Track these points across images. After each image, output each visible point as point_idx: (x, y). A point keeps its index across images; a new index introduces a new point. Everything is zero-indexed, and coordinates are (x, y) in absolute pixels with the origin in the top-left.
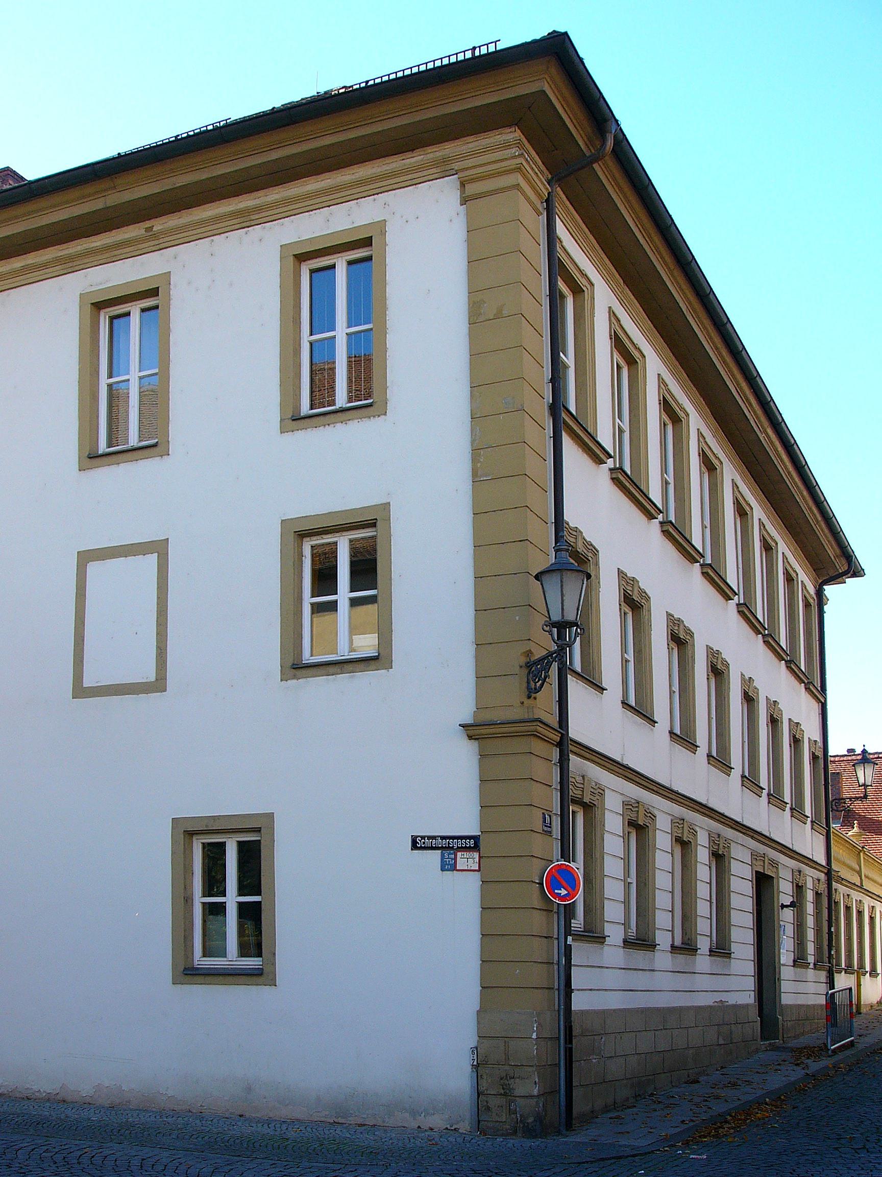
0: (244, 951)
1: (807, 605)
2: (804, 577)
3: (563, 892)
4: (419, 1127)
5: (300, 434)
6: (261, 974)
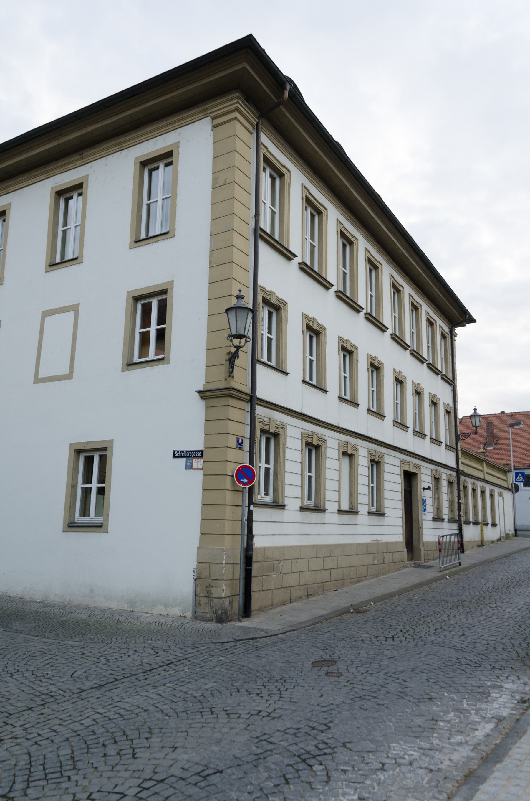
0: (96, 515)
1: (443, 336)
2: (440, 324)
3: (245, 481)
4: (168, 614)
5: (138, 249)
6: (101, 526)
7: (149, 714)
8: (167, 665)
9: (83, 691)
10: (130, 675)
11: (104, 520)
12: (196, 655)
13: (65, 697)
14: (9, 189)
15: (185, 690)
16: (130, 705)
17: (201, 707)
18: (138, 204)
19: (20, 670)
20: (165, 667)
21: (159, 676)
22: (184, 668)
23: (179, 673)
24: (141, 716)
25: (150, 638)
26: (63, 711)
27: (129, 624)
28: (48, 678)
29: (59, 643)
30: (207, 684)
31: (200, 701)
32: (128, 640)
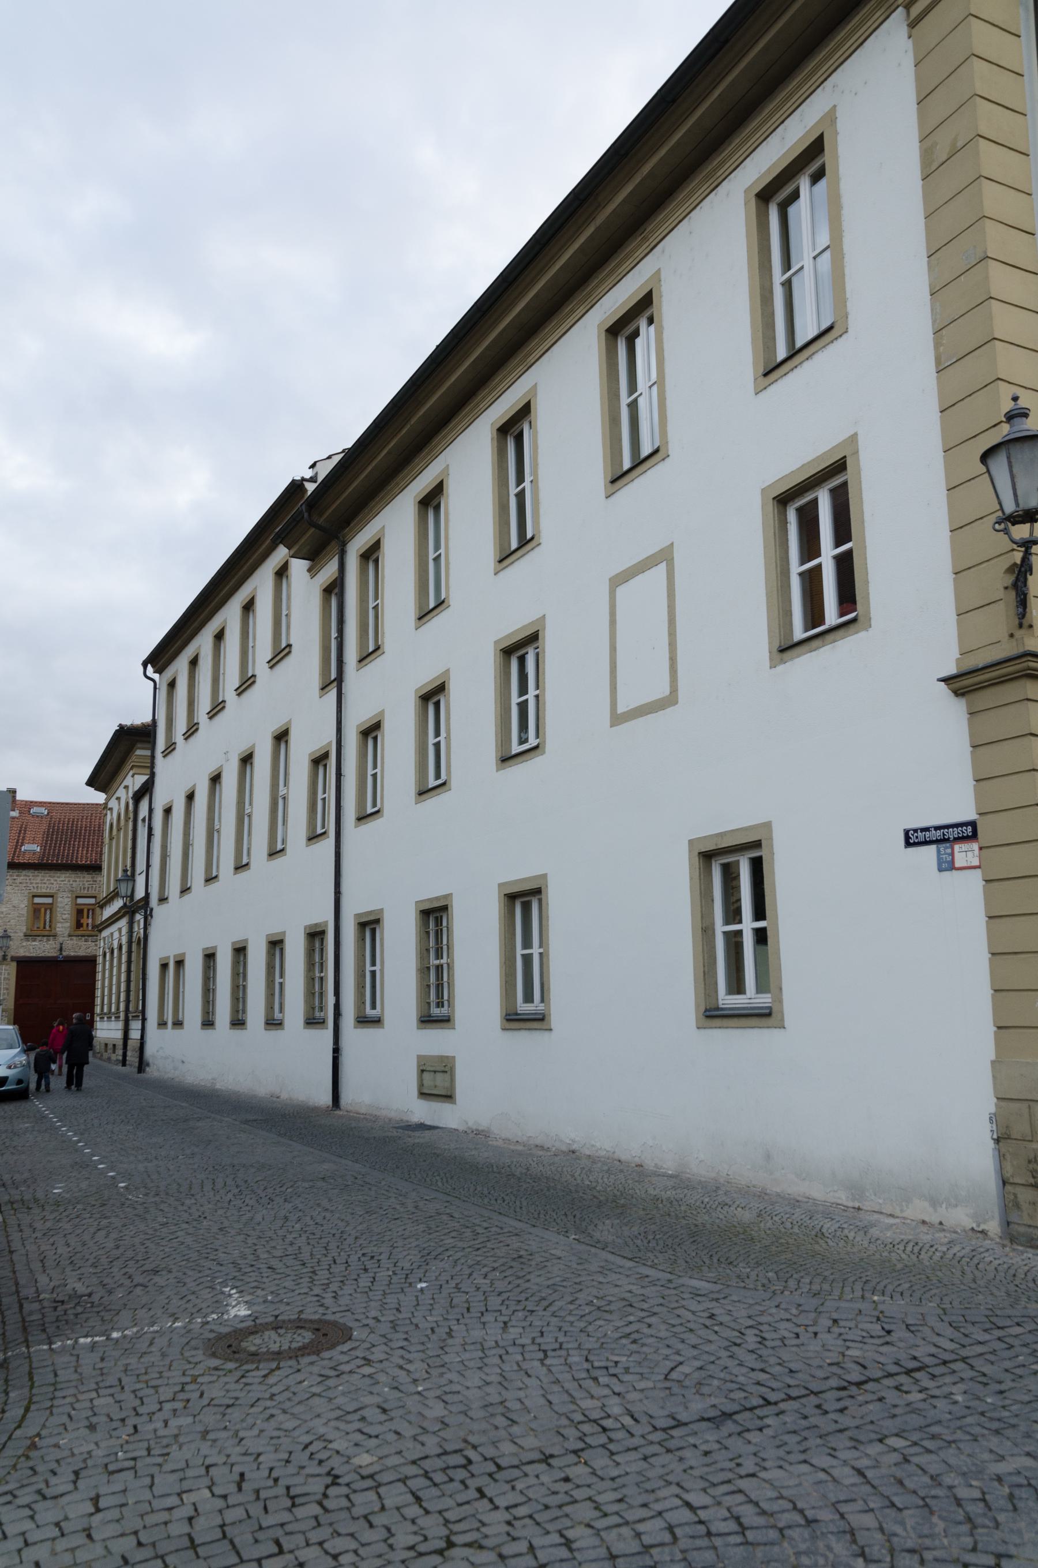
4: (941, 1223)
6: (769, 1015)
7: (814, 1538)
8: (908, 1372)
9: (680, 1424)
10: (804, 1392)
11: (774, 1001)
12: (993, 1352)
13: (632, 1435)
14: (531, 359)
15: (933, 1469)
16: (775, 1494)
17: (968, 1541)
18: (762, 288)
19: (564, 1346)
20: (903, 1379)
21: (878, 1404)
22: (954, 1389)
23: (934, 1401)
24: (792, 1539)
25: (880, 1287)
26: (613, 1479)
27: (842, 1243)
28: (614, 1375)
29: (670, 1281)
30: (1002, 1458)
31: (969, 1519)
32: (826, 1286)
